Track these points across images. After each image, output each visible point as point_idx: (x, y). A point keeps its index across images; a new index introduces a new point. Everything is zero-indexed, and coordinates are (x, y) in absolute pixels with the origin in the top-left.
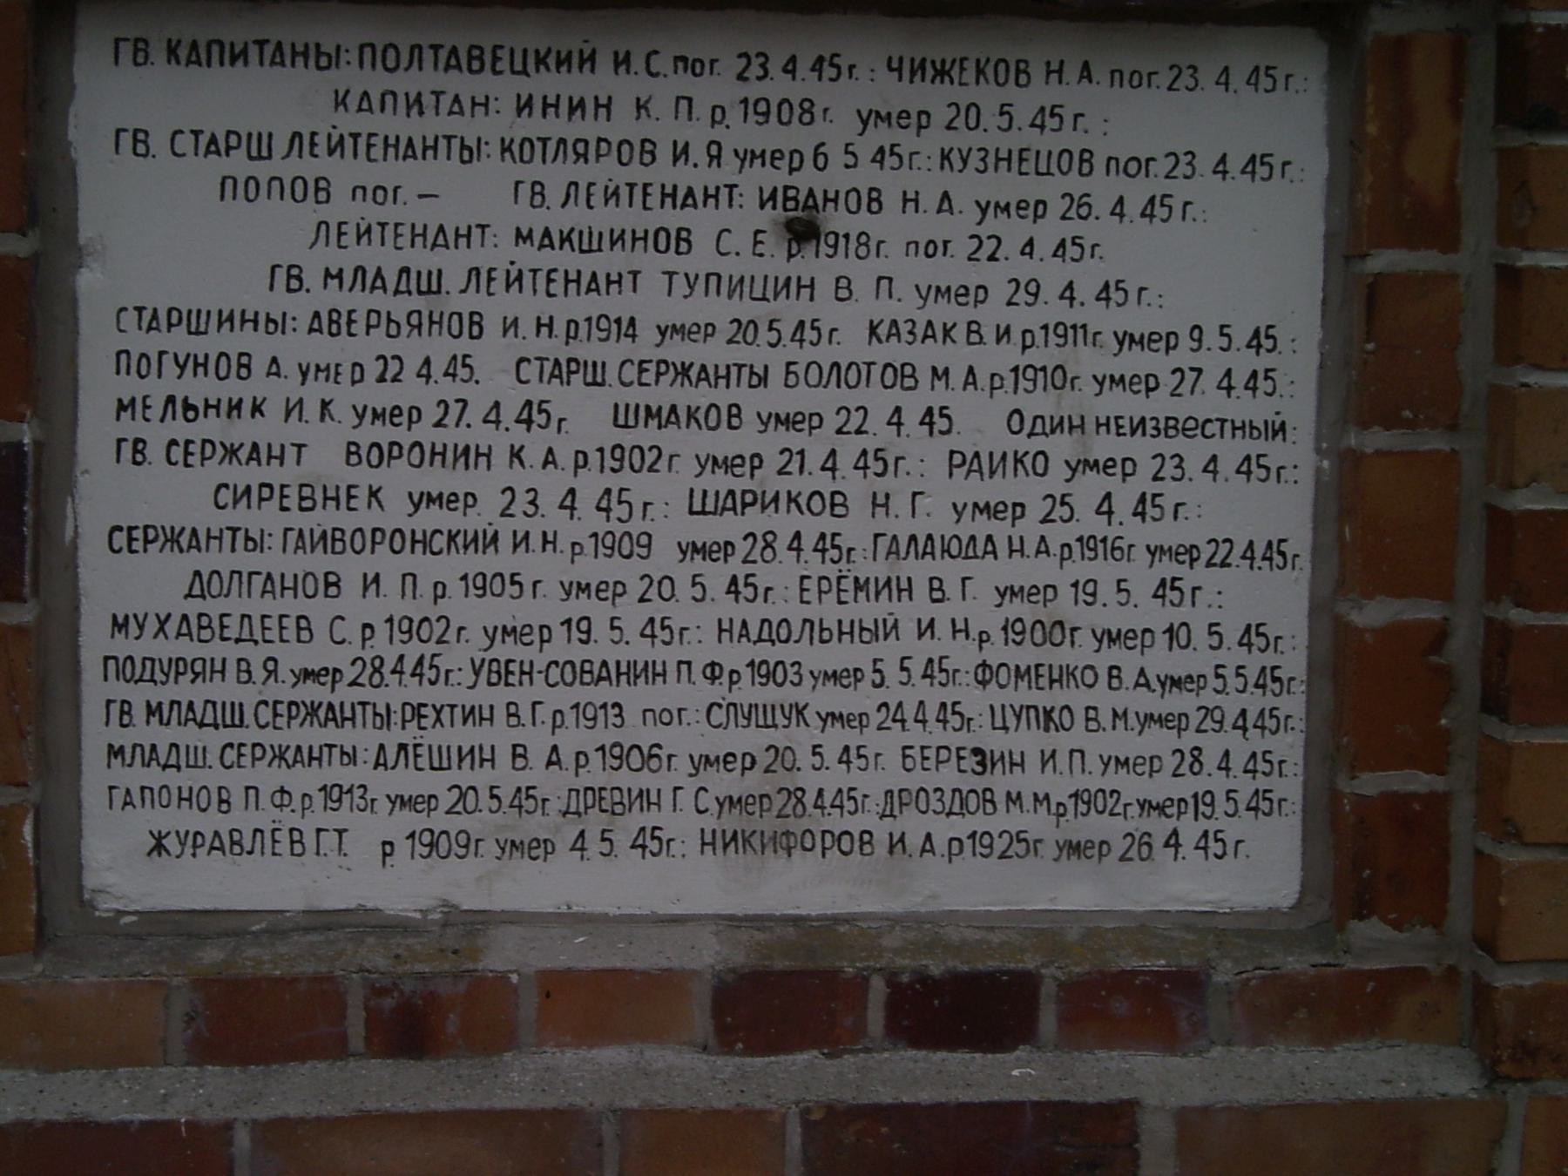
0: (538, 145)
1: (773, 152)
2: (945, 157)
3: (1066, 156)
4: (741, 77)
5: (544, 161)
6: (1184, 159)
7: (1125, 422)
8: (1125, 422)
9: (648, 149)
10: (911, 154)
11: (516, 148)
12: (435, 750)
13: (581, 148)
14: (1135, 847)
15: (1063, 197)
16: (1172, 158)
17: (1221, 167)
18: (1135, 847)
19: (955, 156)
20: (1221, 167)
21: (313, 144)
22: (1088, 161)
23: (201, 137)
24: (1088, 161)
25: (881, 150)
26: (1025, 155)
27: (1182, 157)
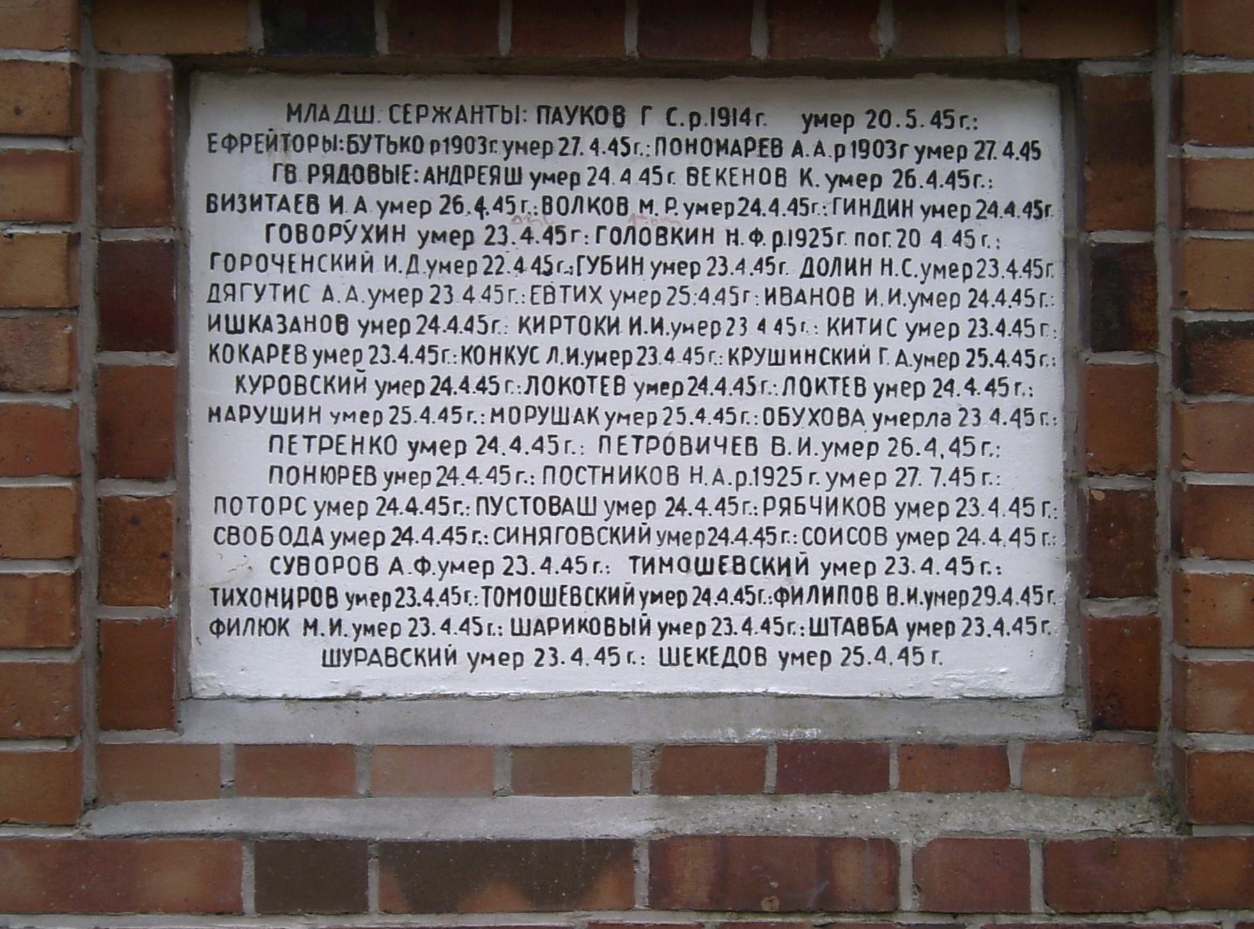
0: (588, 382)
1: (389, 322)
2: (239, 382)
3: (549, 381)
4: (896, 186)
5: (270, 209)
6: (974, 623)
7: (238, 206)
8: (238, 206)
9: (872, 592)
10: (510, 291)
11: (410, 143)
12: (557, 410)
13: (785, 504)
14: (904, 179)
15: (894, 172)
16: (435, 289)
17: (1008, 152)
18: (904, 179)
19: (246, 383)
20: (1008, 152)
21: (722, 564)
22: (302, 353)
23: (274, 199)
24: (302, 353)
25: (760, 261)
26: (738, 441)
27: (974, 622)
